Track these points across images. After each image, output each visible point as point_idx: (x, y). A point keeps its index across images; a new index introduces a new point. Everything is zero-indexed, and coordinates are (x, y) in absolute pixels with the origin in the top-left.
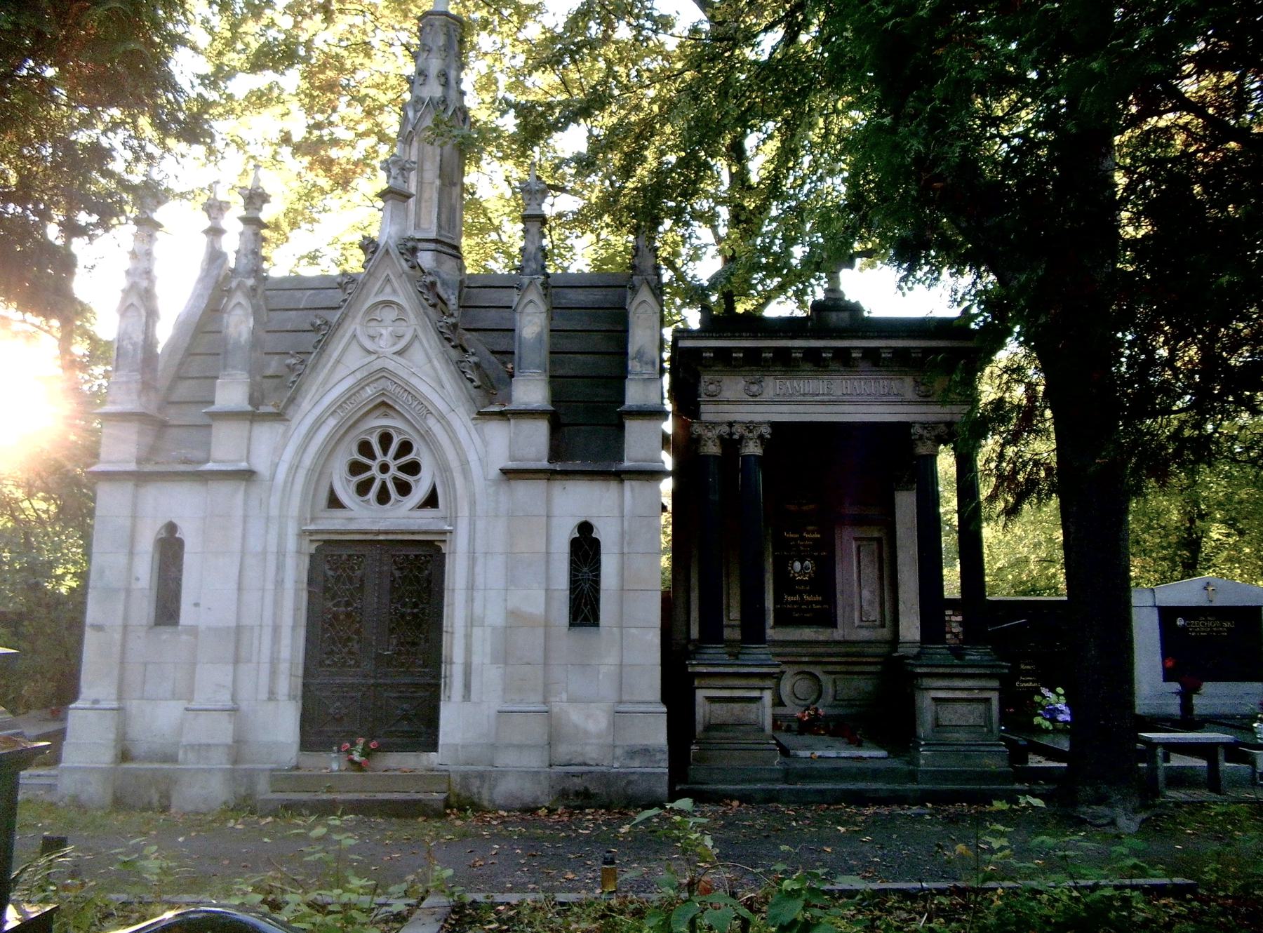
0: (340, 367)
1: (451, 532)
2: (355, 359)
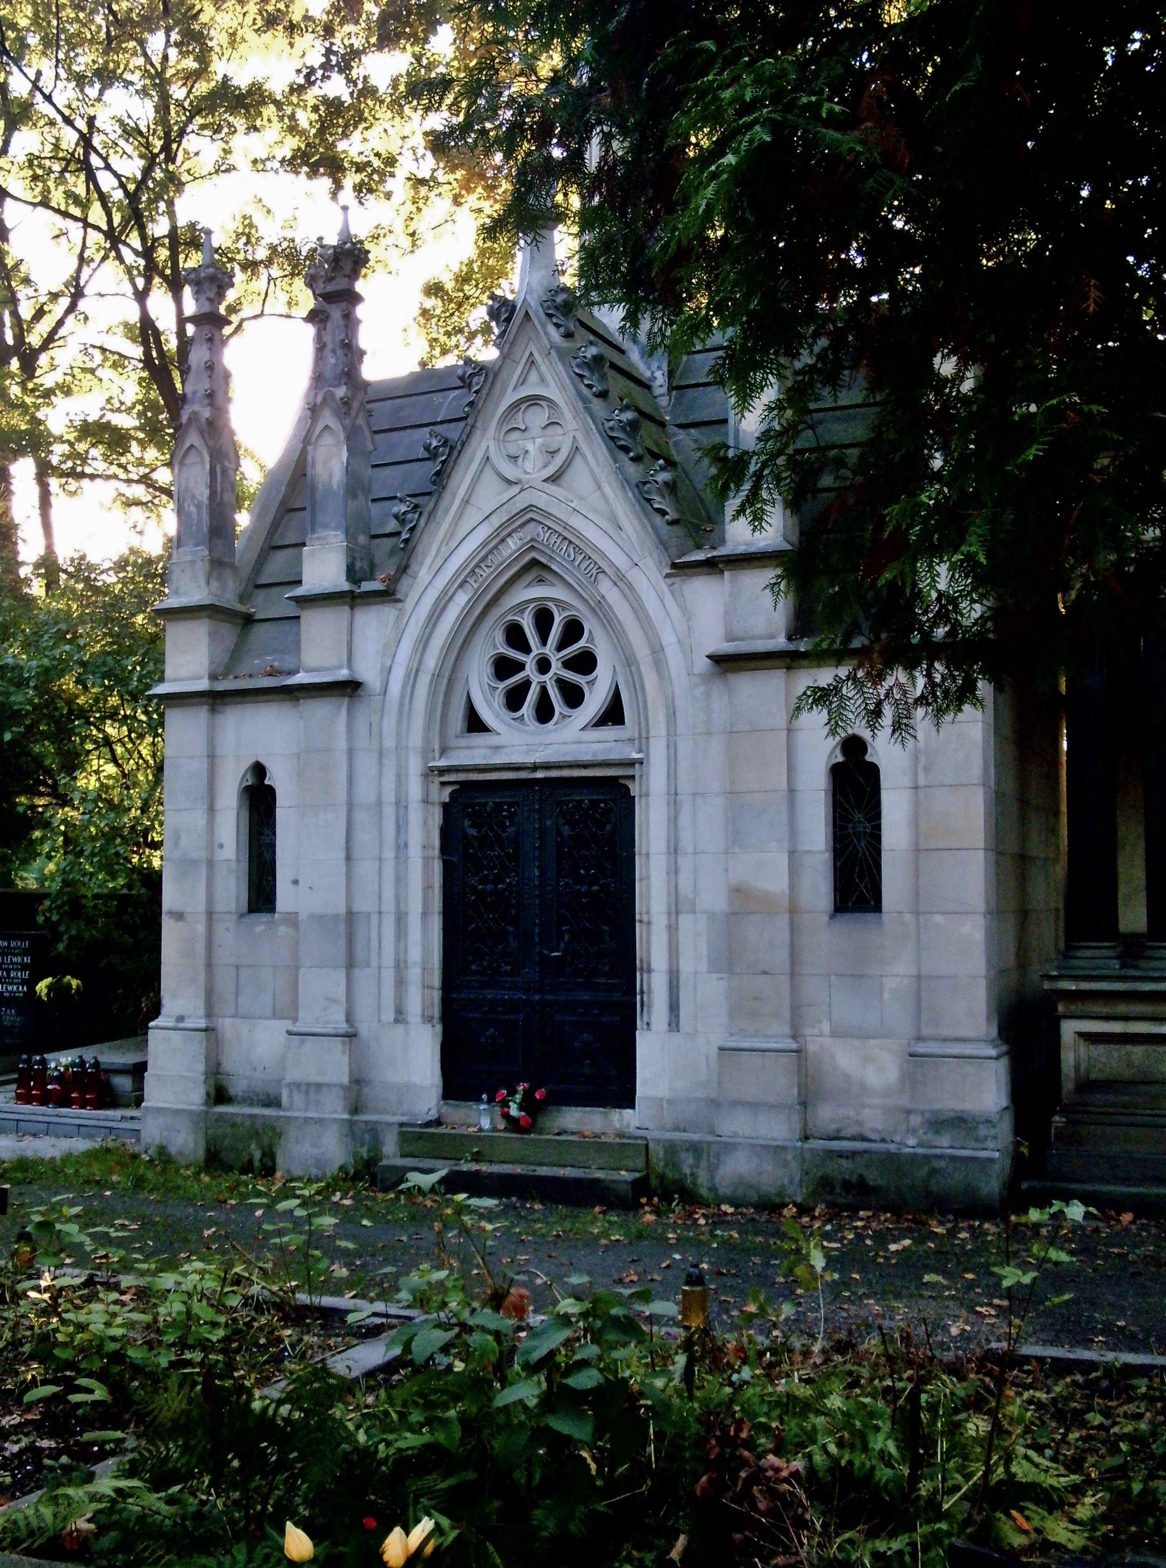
0: (470, 510)
2: (490, 495)
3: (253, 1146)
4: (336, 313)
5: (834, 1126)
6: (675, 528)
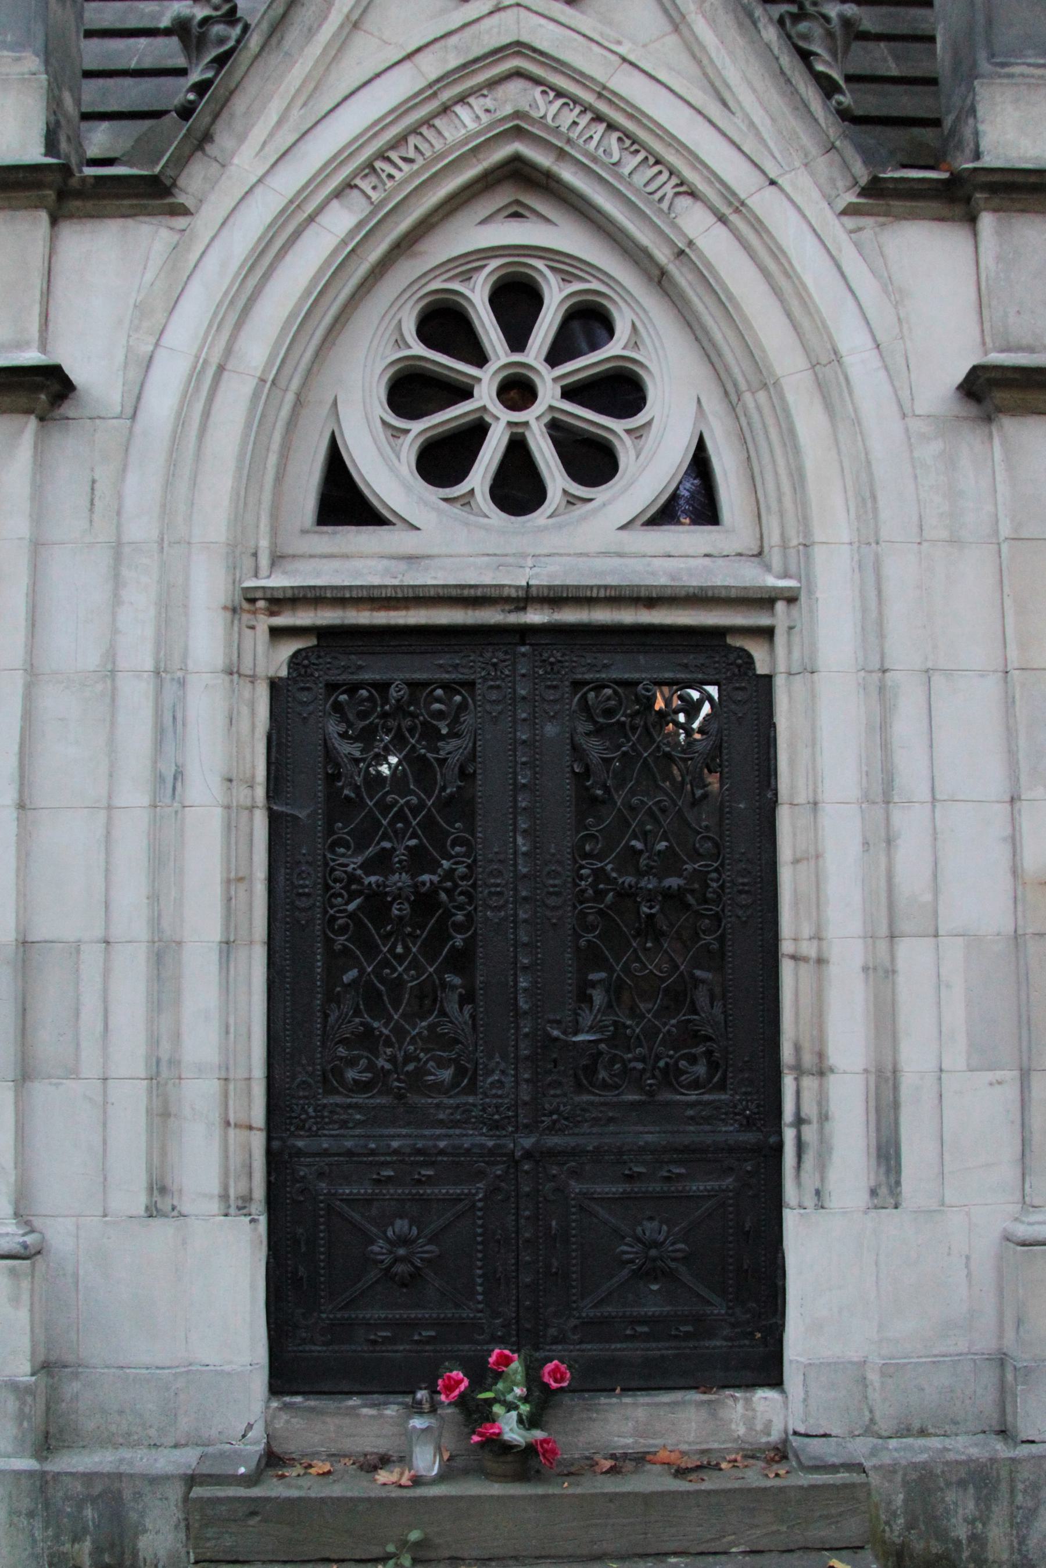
1: (792, 599)
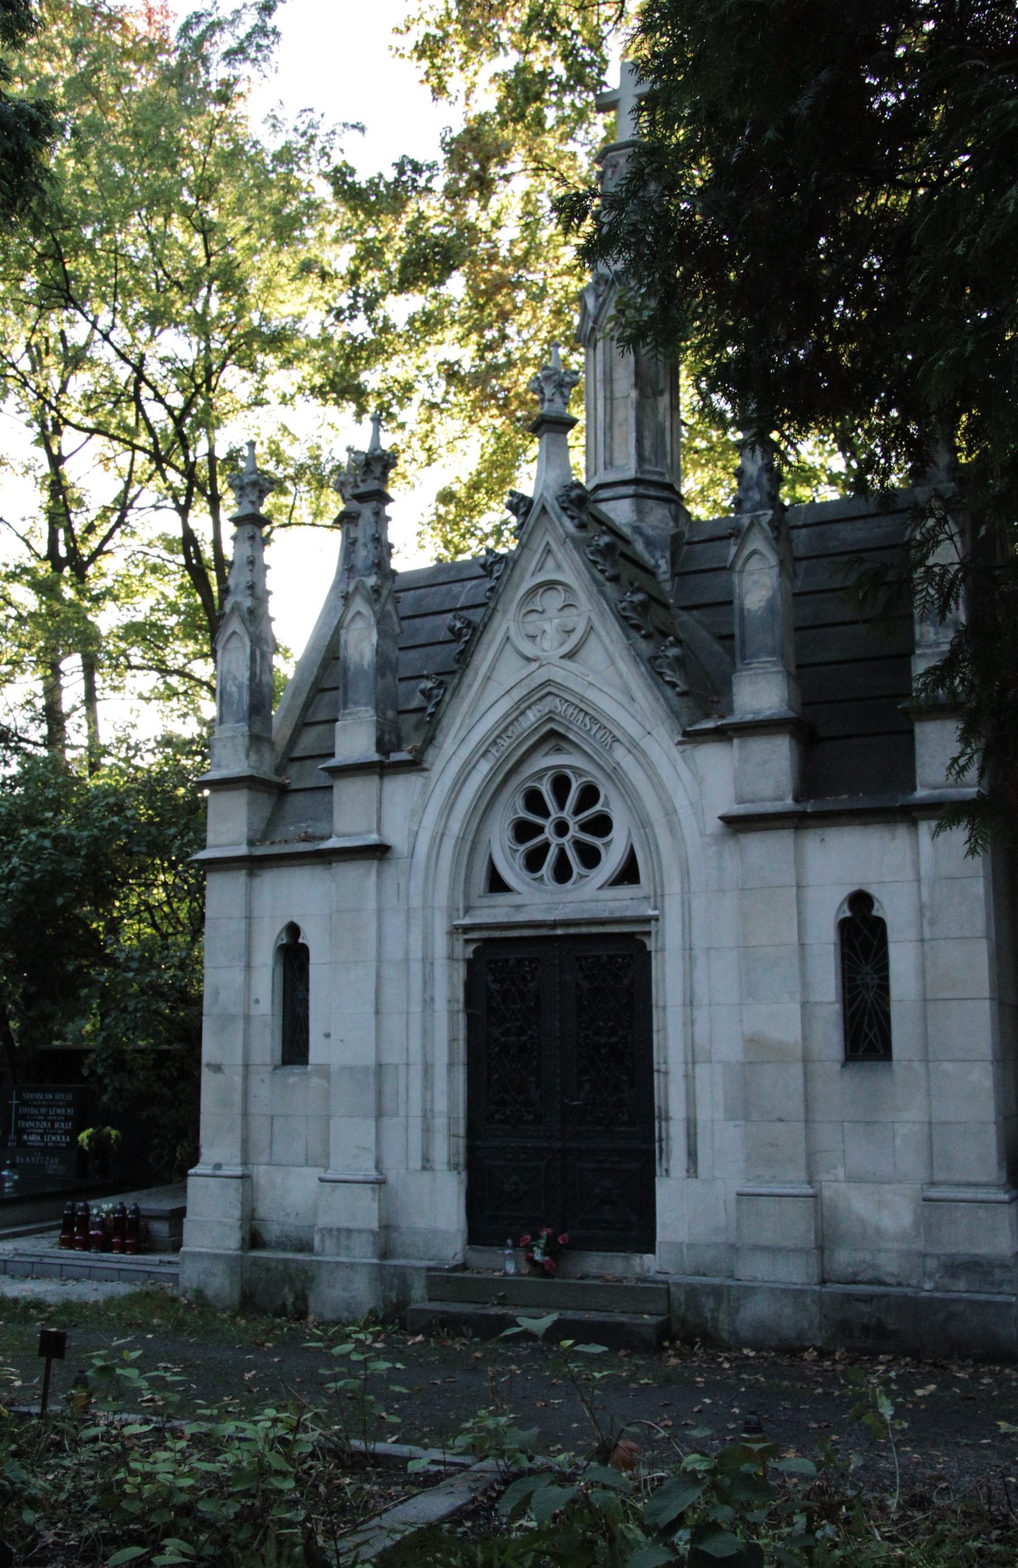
1: (656, 919)
3: (286, 1290)
4: (367, 510)
5: (850, 1270)
6: (685, 699)
